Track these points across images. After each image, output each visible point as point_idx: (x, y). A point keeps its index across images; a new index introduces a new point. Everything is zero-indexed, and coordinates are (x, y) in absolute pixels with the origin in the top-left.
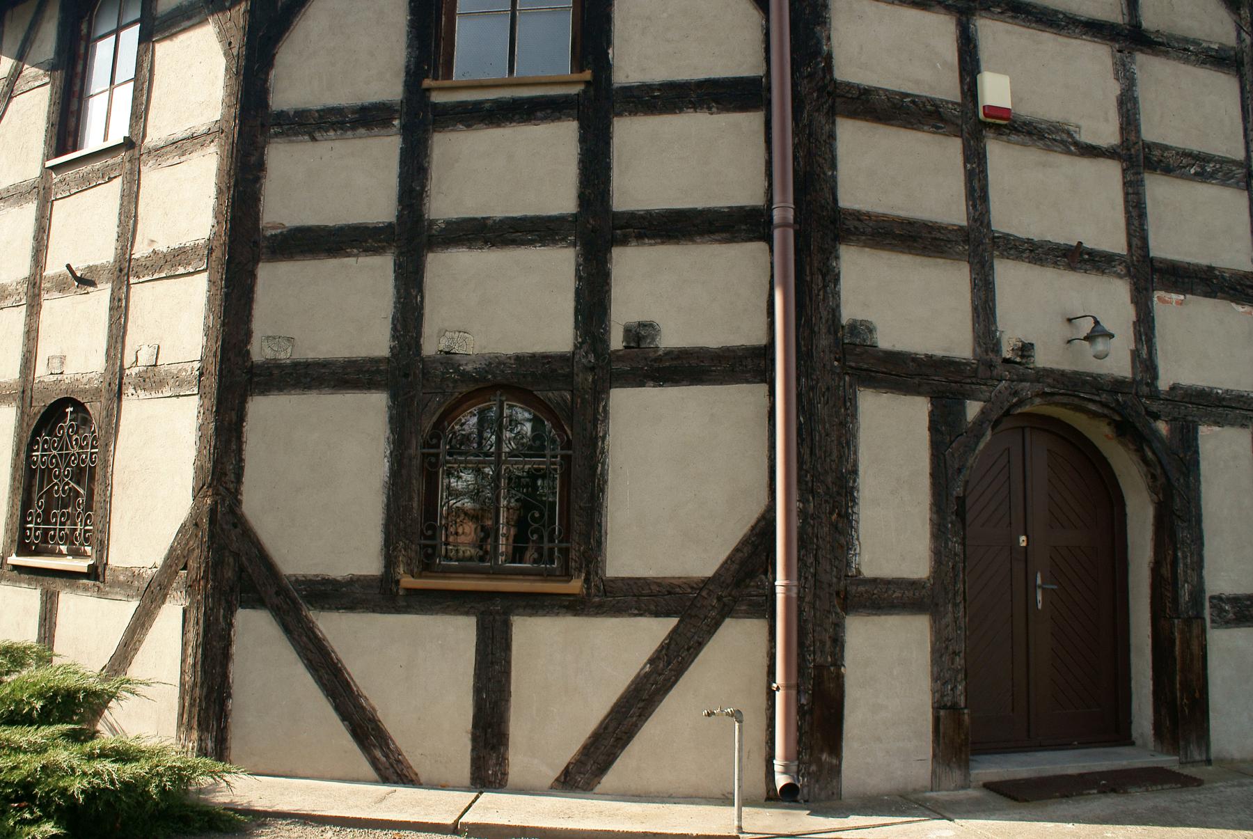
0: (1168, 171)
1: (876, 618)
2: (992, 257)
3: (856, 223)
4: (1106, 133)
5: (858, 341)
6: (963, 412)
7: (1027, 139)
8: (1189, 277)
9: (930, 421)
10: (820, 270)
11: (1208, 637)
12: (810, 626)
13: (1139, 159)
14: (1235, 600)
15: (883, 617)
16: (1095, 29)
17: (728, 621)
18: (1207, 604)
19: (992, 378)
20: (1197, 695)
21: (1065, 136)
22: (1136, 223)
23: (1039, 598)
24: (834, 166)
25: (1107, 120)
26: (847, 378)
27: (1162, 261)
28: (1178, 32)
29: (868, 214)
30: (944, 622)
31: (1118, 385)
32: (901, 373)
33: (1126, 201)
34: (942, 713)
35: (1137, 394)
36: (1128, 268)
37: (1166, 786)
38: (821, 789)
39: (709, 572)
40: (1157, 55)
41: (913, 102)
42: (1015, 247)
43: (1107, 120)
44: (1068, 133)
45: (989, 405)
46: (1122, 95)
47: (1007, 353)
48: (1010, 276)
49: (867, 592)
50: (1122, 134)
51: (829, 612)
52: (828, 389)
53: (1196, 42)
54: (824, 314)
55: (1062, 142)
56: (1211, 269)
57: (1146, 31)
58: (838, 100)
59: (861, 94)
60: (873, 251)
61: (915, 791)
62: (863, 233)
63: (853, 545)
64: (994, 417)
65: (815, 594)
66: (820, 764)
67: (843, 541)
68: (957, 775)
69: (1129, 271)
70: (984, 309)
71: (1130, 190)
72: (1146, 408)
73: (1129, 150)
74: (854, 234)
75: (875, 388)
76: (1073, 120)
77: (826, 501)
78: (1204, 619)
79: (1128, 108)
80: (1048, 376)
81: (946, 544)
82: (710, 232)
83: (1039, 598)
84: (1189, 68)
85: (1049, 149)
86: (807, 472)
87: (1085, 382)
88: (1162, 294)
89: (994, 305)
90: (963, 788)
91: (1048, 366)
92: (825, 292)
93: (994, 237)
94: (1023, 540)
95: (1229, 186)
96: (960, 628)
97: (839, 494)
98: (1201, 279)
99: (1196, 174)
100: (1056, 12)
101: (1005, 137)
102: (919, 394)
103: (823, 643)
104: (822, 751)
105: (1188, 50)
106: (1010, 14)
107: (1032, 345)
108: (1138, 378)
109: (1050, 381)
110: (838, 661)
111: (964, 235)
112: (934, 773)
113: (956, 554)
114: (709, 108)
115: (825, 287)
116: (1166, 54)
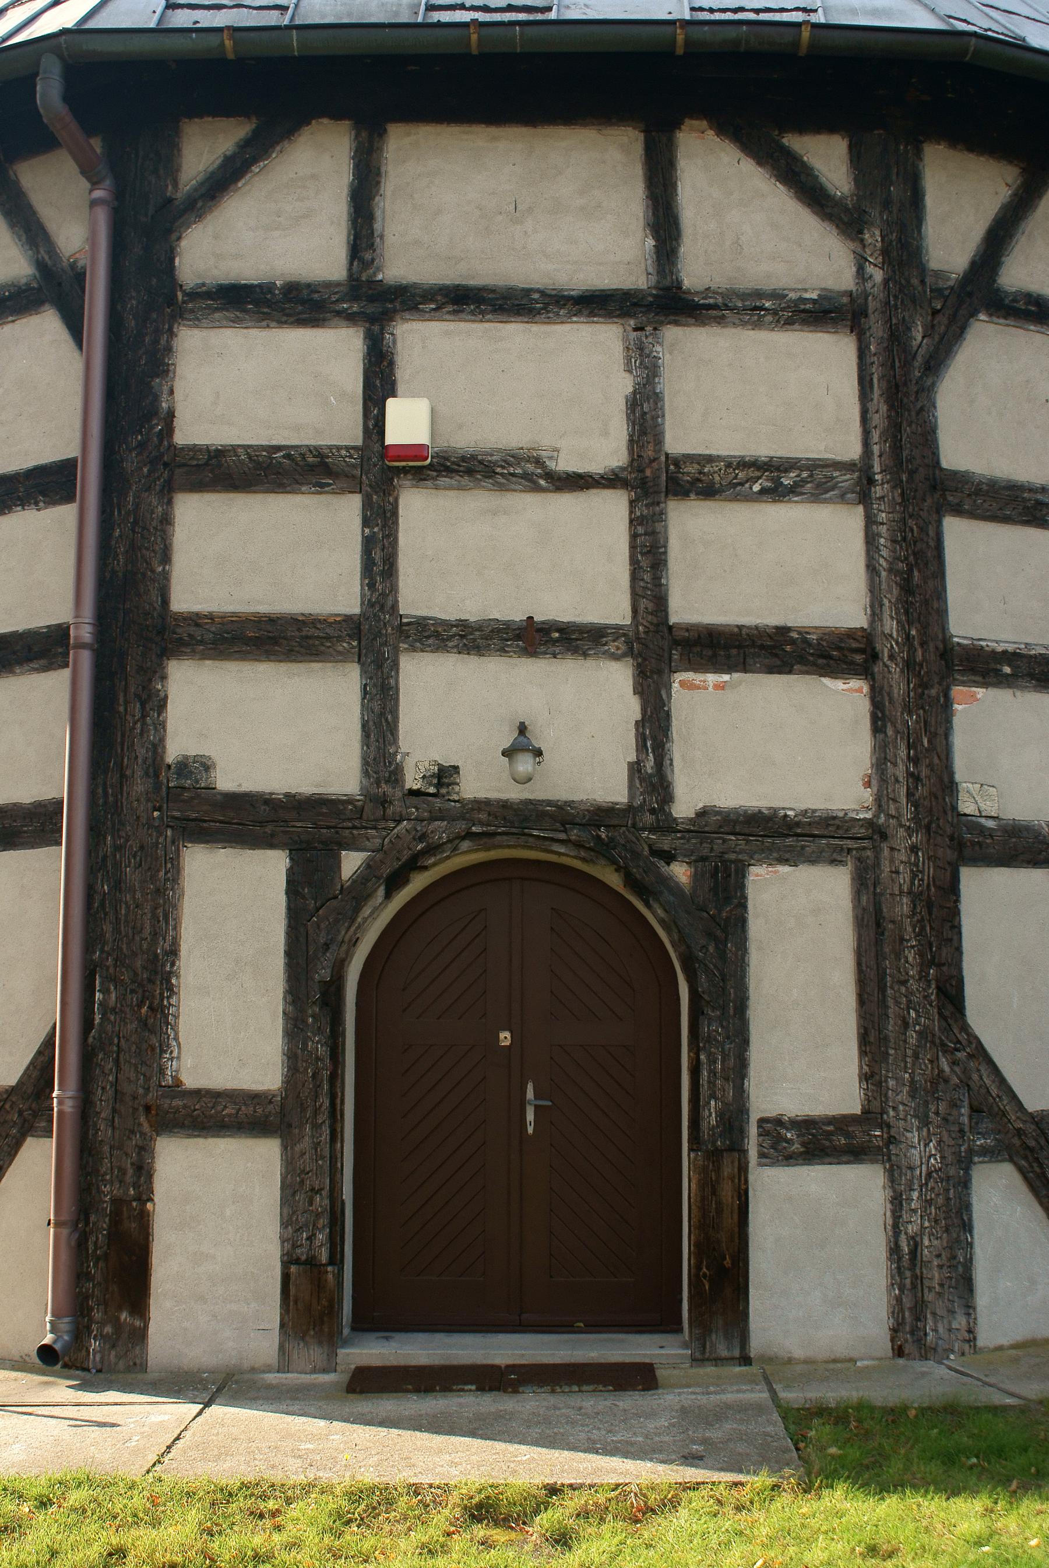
0: (709, 492)
1: (200, 1141)
2: (396, 651)
3: (192, 629)
4: (607, 449)
5: (188, 783)
6: (336, 866)
7: (465, 480)
8: (739, 647)
9: (288, 882)
10: (138, 696)
11: (751, 1178)
12: (106, 1148)
13: (656, 480)
14: (806, 1125)
15: (211, 1141)
16: (594, 304)
17: (30, 1141)
18: (753, 1130)
19: (385, 818)
20: (728, 1262)
21: (530, 467)
22: (647, 577)
23: (530, 1116)
24: (166, 557)
25: (605, 433)
26: (169, 833)
27: (689, 628)
28: (746, 284)
29: (211, 616)
30: (298, 1148)
31: (601, 815)
32: (247, 820)
33: (633, 547)
34: (293, 1269)
35: (634, 826)
36: (629, 643)
37: (585, 1388)
38: (118, 1357)
39: (13, 1081)
40: (703, 324)
41: (288, 456)
42: (437, 635)
43: (605, 433)
44: (538, 462)
45: (379, 856)
46: (634, 393)
47: (412, 781)
48: (421, 675)
49: (185, 1106)
50: (631, 450)
51: (132, 1132)
52: (142, 848)
53: (776, 295)
54: (141, 752)
55: (526, 476)
56: (783, 631)
57: (688, 292)
58: (178, 471)
59: (210, 458)
60: (217, 663)
61: (253, 1370)
62: (202, 642)
63: (168, 1046)
64: (386, 871)
65: (114, 1111)
66: (118, 1326)
67: (154, 1041)
68: (317, 1353)
69: (631, 649)
70: (378, 725)
71: (640, 530)
72: (650, 846)
73: (642, 471)
74: (187, 645)
75: (207, 842)
76: (546, 441)
77: (132, 991)
78: (744, 1152)
79: (644, 413)
80: (479, 810)
81: (305, 1045)
82: (30, 660)
83: (530, 1116)
84: (763, 335)
85: (502, 488)
86: (109, 954)
87: (543, 814)
88: (689, 676)
89: (396, 719)
90: (324, 1371)
91: (482, 795)
92: (144, 724)
93: (401, 624)
94: (505, 1038)
95: (826, 501)
96: (322, 1158)
97: (151, 981)
98: (762, 647)
99: (763, 491)
100: (528, 292)
101: (429, 483)
102: (272, 846)
103: (123, 1171)
104: (120, 1309)
105: (761, 308)
106: (450, 308)
107: (456, 769)
108: (637, 802)
109: (483, 816)
110: (145, 1194)
111: (352, 626)
112: (281, 1347)
113: (318, 1059)
114: (36, 504)
115: (144, 717)
116: (721, 321)
